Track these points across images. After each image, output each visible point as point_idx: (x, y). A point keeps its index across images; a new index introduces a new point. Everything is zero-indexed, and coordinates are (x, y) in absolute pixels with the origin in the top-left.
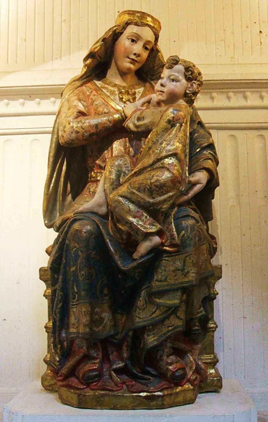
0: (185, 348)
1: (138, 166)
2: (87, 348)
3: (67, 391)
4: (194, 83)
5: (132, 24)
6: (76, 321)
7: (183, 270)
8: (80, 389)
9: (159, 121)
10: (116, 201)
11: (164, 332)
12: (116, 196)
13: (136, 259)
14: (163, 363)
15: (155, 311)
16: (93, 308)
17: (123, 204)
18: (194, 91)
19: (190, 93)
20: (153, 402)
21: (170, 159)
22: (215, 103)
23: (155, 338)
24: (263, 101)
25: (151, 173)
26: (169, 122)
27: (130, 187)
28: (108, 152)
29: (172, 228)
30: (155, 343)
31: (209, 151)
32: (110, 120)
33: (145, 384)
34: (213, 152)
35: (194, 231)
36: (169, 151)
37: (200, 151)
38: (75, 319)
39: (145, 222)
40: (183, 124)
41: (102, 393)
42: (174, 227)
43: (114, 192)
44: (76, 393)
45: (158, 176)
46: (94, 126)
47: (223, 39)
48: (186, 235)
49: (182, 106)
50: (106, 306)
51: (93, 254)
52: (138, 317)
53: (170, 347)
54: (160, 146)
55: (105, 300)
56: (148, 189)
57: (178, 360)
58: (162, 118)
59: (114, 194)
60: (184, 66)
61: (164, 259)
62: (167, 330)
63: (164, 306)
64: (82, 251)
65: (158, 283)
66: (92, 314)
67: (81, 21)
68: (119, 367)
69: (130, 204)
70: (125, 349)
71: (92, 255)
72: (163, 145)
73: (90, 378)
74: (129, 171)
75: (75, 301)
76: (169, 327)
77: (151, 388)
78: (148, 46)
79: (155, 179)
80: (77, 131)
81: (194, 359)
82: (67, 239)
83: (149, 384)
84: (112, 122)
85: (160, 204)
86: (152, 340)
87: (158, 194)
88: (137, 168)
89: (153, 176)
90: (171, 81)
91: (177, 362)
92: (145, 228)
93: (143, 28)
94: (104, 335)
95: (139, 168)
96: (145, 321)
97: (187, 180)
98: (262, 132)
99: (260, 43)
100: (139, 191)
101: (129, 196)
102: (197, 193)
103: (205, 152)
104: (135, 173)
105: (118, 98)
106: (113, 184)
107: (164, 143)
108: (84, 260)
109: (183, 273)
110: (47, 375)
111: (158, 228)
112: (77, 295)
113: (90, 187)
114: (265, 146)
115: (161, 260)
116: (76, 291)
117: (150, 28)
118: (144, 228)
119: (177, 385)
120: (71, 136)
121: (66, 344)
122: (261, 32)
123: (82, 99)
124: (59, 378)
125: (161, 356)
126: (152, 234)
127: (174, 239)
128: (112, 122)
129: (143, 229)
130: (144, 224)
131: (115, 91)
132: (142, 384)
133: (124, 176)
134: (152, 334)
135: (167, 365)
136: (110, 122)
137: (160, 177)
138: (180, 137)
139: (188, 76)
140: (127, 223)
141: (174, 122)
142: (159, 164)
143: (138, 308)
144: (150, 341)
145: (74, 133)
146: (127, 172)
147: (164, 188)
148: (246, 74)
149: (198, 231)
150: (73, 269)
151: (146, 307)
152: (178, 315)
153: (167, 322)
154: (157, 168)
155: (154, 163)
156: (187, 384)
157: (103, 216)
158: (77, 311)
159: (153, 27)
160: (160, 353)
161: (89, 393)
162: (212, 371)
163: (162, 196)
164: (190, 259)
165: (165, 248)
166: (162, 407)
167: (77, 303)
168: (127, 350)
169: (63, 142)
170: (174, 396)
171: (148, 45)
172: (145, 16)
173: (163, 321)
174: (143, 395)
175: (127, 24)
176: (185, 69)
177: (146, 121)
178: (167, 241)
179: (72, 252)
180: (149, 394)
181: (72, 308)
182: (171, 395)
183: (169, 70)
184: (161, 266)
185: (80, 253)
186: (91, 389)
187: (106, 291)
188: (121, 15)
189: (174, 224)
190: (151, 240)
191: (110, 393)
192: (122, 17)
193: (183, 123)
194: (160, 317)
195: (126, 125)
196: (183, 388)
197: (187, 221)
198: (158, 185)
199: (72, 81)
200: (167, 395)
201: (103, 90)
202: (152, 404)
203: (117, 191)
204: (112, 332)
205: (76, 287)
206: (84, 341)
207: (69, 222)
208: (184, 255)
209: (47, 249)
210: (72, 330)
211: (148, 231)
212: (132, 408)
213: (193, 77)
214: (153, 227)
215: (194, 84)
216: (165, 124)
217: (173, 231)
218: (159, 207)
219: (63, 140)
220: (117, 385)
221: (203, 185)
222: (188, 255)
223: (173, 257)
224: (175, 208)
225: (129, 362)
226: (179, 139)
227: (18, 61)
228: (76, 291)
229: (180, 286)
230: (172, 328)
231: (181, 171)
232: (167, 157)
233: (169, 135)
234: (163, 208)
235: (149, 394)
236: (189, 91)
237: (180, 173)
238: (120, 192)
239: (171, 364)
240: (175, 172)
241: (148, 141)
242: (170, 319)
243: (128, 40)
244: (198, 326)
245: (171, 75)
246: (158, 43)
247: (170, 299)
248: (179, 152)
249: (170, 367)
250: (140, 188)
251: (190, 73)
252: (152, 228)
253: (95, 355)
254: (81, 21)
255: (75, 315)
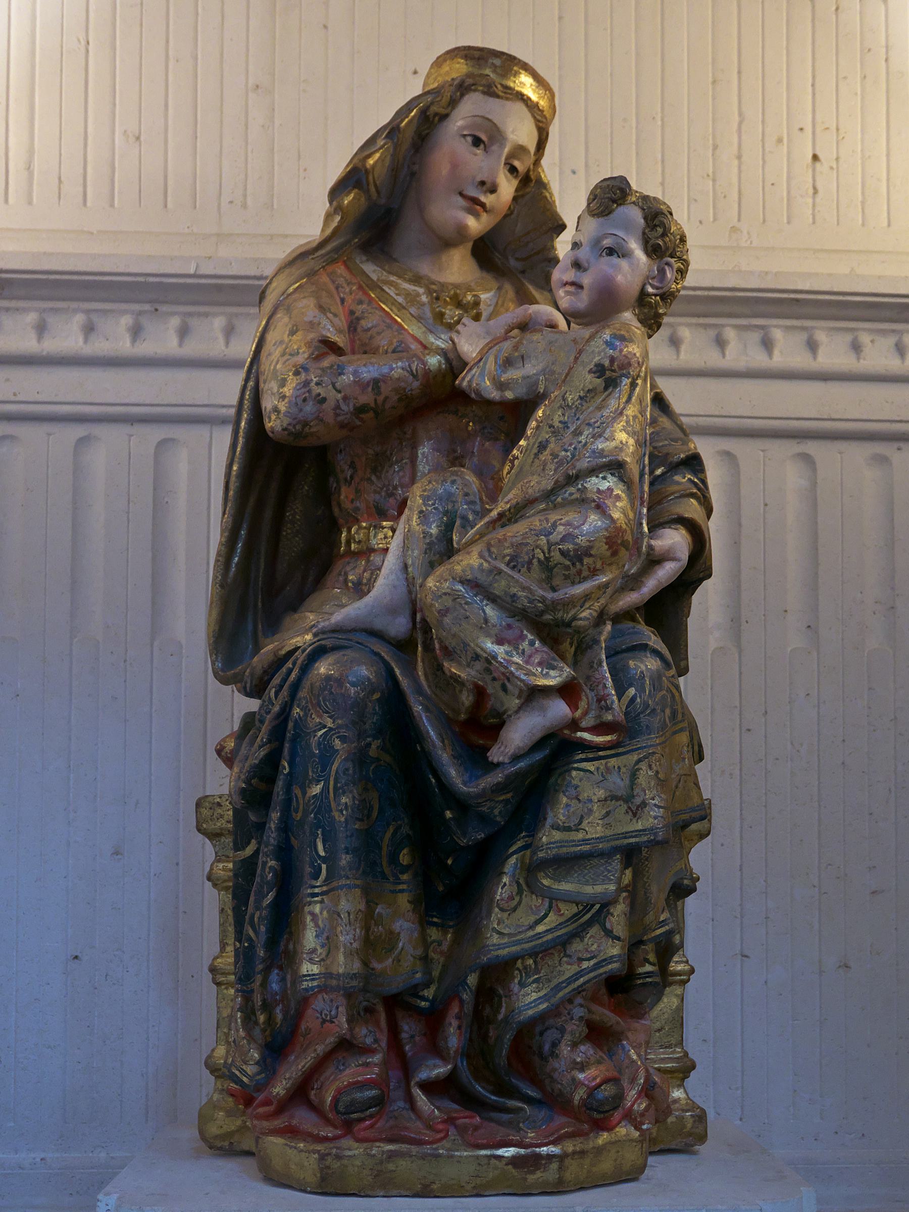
0: (618, 1023)
1: (510, 496)
2: (349, 1021)
3: (286, 1145)
4: (668, 264)
5: (475, 91)
6: (322, 940)
7: (628, 799)
8: (326, 1139)
9: (571, 369)
10: (445, 594)
11: (568, 975)
12: (446, 580)
13: (498, 765)
14: (559, 1065)
15: (546, 916)
16: (371, 904)
17: (467, 603)
18: (664, 290)
19: (656, 295)
20: (533, 1172)
21: (604, 478)
22: (682, 356)
23: (541, 994)
24: (815, 358)
25: (549, 517)
26: (600, 370)
27: (486, 554)
28: (402, 469)
29: (604, 677)
30: (543, 1006)
31: (689, 476)
32: (414, 369)
33: (509, 1124)
34: (698, 479)
35: (661, 690)
36: (601, 454)
37: (663, 474)
38: (317, 936)
39: (530, 656)
40: (639, 382)
41: (391, 1151)
42: (608, 675)
43: (440, 570)
44: (314, 1152)
45: (568, 524)
46: (368, 383)
47: (711, 174)
48: (638, 700)
49: (633, 328)
50: (403, 901)
51: (374, 746)
52: (499, 933)
53: (581, 1017)
54: (575, 441)
55: (403, 883)
56: (539, 560)
57: (601, 1057)
58: (580, 359)
59: (441, 576)
60: (644, 209)
61: (576, 765)
62: (574, 969)
63: (568, 899)
64: (343, 739)
65: (557, 835)
66: (368, 918)
67: (304, 91)
68: (437, 1076)
69: (487, 605)
70: (455, 1023)
71: (373, 752)
72: (582, 438)
73: (353, 1107)
74: (475, 512)
75: (318, 884)
76: (580, 960)
77: (530, 1135)
78: (516, 163)
79: (559, 533)
80: (319, 395)
81: (639, 1055)
82: (296, 702)
83: (523, 1122)
84: (420, 377)
85: (574, 606)
86: (533, 998)
87: (567, 577)
88: (507, 503)
89: (554, 525)
90: (604, 254)
91: (599, 1062)
92: (529, 673)
93: (508, 103)
94: (395, 985)
95: (514, 502)
96: (518, 943)
97: (645, 543)
98: (811, 447)
99: (811, 191)
100: (514, 567)
101: (483, 579)
102: (666, 585)
103: (677, 478)
104: (501, 515)
105: (429, 314)
106: (430, 549)
107: (586, 433)
108: (350, 765)
109: (629, 808)
110: (215, 1107)
111: (565, 674)
112: (324, 866)
113: (348, 568)
114: (814, 484)
115: (569, 771)
116: (322, 853)
117: (527, 105)
118: (525, 674)
119: (601, 1125)
120: (301, 410)
121: (282, 1010)
122: (815, 158)
123: (329, 309)
124: (261, 1110)
125: (555, 1045)
126: (545, 691)
127: (608, 708)
128: (420, 377)
129: (523, 677)
130: (527, 662)
131: (418, 295)
132: (499, 1123)
133: (463, 526)
134: (533, 982)
135: (572, 1069)
136: (415, 376)
137: (575, 529)
138: (631, 418)
139: (651, 242)
140: (477, 657)
141: (614, 371)
142: (571, 491)
143: (498, 906)
144: (529, 999)
145: (311, 403)
146: (471, 517)
147: (586, 560)
148: (777, 274)
149: (669, 690)
150: (316, 789)
151: (520, 903)
152: (608, 925)
153: (576, 947)
154: (568, 504)
155: (558, 487)
156: (623, 1123)
157: (399, 641)
158: (325, 913)
159: (536, 105)
160: (550, 1035)
161: (353, 1149)
162: (677, 1094)
163: (580, 582)
164: (650, 767)
165: (579, 734)
166: (557, 1188)
167: (325, 888)
168: (459, 1028)
169: (279, 428)
170: (591, 1156)
171: (519, 159)
172: (515, 68)
173: (562, 944)
174: (506, 1155)
175: (463, 88)
176: (645, 218)
177: (530, 369)
178: (586, 713)
179: (314, 742)
180: (522, 1151)
181: (310, 903)
182: (583, 1153)
183: (601, 219)
184: (567, 786)
185: (337, 743)
186: (358, 1140)
187: (405, 857)
188: (445, 61)
189: (608, 664)
190: (543, 709)
191: (414, 1149)
192: (446, 68)
193: (638, 376)
194: (559, 933)
195: (465, 384)
196: (613, 1135)
197: (642, 662)
198: (568, 550)
199: (295, 255)
200: (574, 1153)
201: (386, 288)
202: (531, 1178)
203: (449, 567)
204: (418, 975)
205: (324, 842)
206: (342, 1000)
207: (301, 657)
208: (635, 757)
209: (219, 743)
210: (308, 968)
211: (540, 684)
212: (475, 1192)
213: (665, 243)
214: (552, 673)
215: (666, 268)
216: (589, 377)
217: (605, 684)
218: (570, 615)
219: (278, 421)
220: (430, 1127)
221: (682, 563)
222: (645, 757)
223: (603, 762)
224: (605, 624)
225: (463, 1065)
226: (627, 422)
227: (116, 202)
228: (322, 853)
229: (618, 843)
230: (592, 962)
231: (631, 515)
232: (593, 471)
233: (599, 408)
234: (581, 619)
235: (522, 1151)
236: (653, 286)
237: (629, 521)
238: (458, 568)
239: (582, 1067)
240: (616, 515)
241: (538, 427)
242: (586, 940)
243: (462, 139)
244: (654, 965)
245: (605, 236)
246: (543, 162)
247: (587, 881)
248: (628, 459)
249: (581, 1076)
250: (516, 556)
251: (660, 230)
252: (547, 673)
253: (369, 1041)
254: (304, 91)
255: (317, 925)
